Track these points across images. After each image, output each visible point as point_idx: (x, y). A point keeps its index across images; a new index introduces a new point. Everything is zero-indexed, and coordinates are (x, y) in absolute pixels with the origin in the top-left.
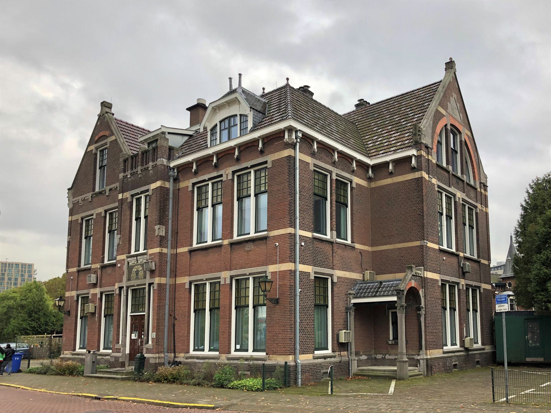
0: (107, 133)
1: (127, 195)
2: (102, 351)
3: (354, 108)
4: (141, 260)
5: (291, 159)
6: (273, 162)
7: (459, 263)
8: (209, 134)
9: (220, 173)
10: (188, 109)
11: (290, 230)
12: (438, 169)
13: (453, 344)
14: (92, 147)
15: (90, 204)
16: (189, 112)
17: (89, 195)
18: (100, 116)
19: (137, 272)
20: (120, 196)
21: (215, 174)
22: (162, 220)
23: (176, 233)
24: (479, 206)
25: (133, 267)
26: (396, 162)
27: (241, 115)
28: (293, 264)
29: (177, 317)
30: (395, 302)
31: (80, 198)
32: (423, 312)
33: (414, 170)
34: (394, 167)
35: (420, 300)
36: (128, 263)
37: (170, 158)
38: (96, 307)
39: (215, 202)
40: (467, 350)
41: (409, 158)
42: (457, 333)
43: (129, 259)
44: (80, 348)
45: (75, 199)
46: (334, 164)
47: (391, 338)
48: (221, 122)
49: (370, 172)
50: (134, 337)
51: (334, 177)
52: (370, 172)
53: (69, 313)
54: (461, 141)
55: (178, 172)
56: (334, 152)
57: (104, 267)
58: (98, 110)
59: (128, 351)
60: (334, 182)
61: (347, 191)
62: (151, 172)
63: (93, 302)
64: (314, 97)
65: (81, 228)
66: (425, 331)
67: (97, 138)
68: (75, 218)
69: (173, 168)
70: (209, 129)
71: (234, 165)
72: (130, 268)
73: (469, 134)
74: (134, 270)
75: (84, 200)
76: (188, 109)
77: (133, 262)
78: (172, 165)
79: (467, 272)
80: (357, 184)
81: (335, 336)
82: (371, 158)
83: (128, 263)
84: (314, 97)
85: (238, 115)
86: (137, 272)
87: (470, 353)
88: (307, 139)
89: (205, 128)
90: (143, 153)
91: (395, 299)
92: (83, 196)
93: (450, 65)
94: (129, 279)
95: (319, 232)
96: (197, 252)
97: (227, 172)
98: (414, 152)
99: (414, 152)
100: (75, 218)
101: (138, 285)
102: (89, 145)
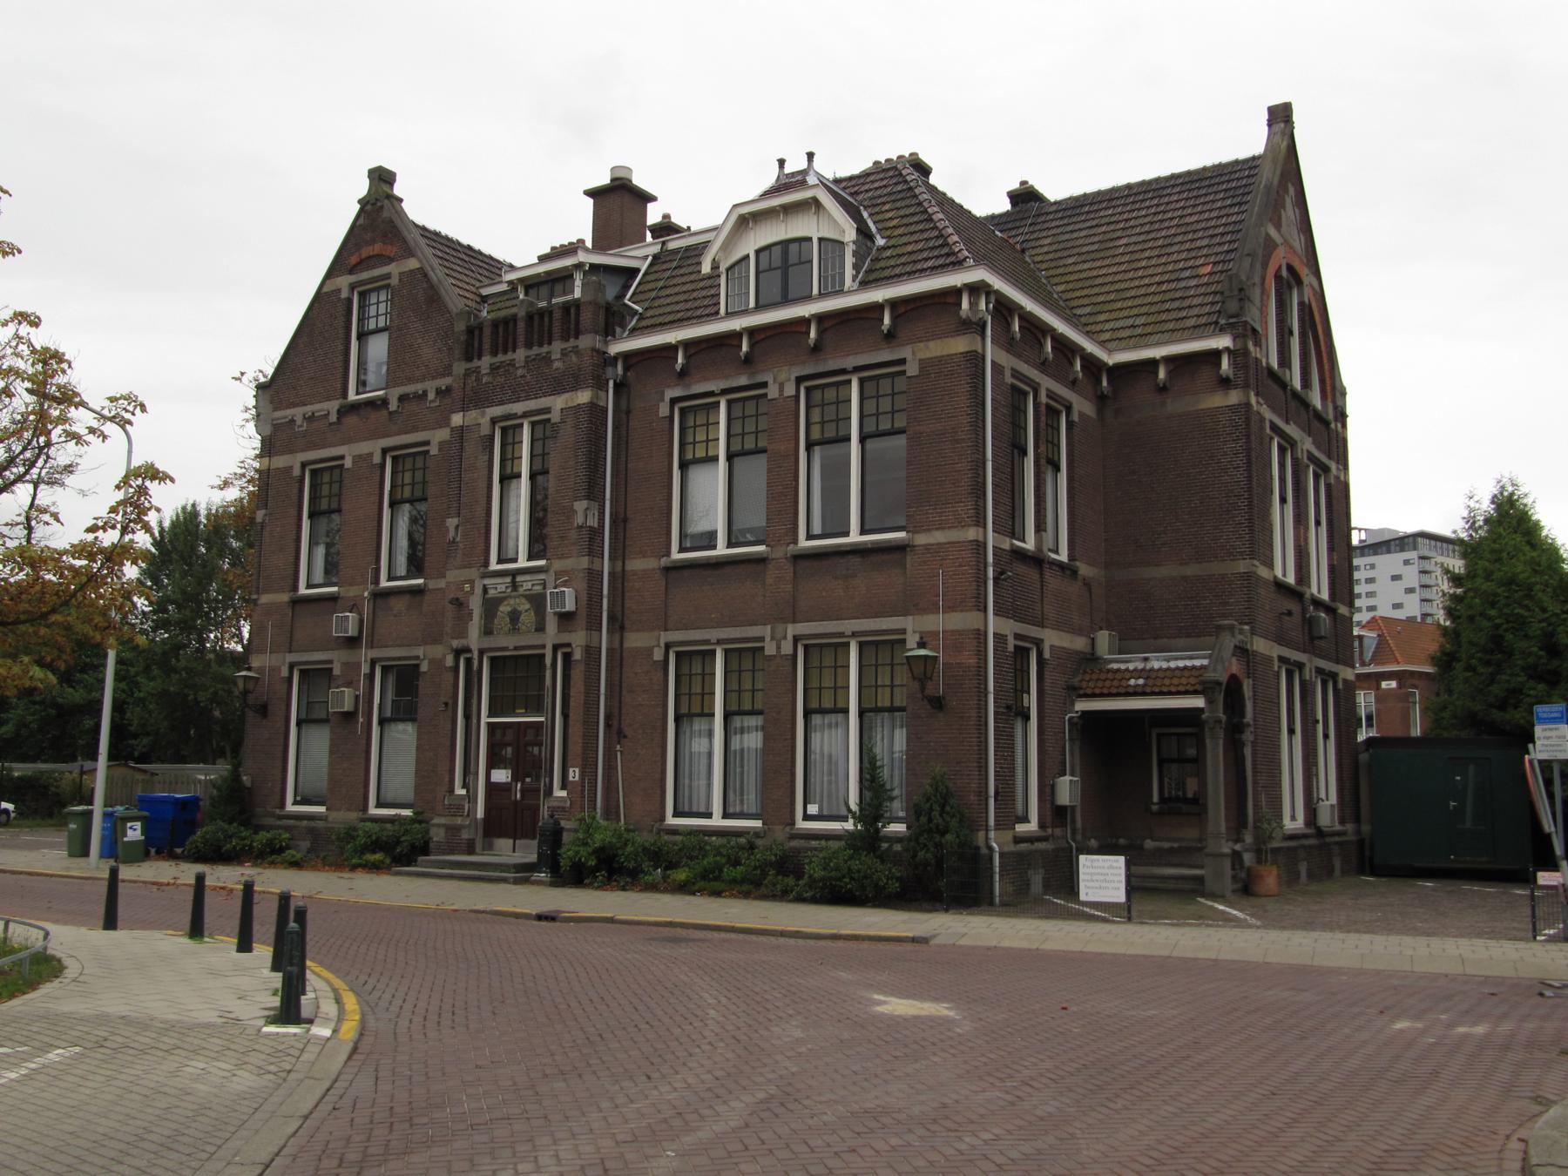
0: (390, 250)
1: (481, 418)
2: (290, 807)
3: (1004, 206)
4: (527, 586)
5: (976, 359)
6: (924, 365)
7: (1304, 611)
8: (723, 278)
9: (760, 379)
10: (590, 193)
11: (972, 534)
12: (1270, 382)
13: (1293, 818)
14: (344, 282)
15: (318, 431)
16: (591, 201)
17: (333, 406)
18: (363, 202)
19: (514, 616)
20: (457, 419)
21: (743, 381)
22: (593, 491)
23: (620, 521)
24: (1333, 466)
25: (498, 601)
26: (1178, 363)
27: (820, 240)
28: (981, 615)
29: (627, 731)
30: (1201, 710)
31: (298, 413)
32: (1248, 736)
33: (1225, 383)
34: (1169, 373)
35: (1243, 706)
36: (485, 590)
37: (608, 332)
38: (357, 697)
39: (736, 447)
40: (1320, 833)
41: (1215, 355)
42: (1304, 789)
43: (487, 581)
44: (295, 803)
45: (278, 414)
46: (1043, 366)
47: (1156, 799)
48: (758, 252)
49: (1105, 383)
50: (501, 776)
51: (1043, 399)
52: (1105, 383)
53: (263, 710)
54: (1301, 304)
55: (626, 369)
56: (1044, 336)
57: (381, 596)
58: (362, 187)
59: (480, 814)
60: (1043, 409)
61: (1058, 430)
62: (557, 365)
63: (349, 684)
64: (933, 180)
65: (301, 491)
66: (1255, 783)
67: (354, 260)
68: (280, 462)
69: (615, 358)
70: (723, 268)
71: (804, 363)
72: (491, 606)
73: (1316, 284)
74: (504, 609)
75: (310, 419)
76: (590, 193)
77: (502, 588)
78: (616, 348)
79: (1321, 638)
80: (1081, 414)
81: (1048, 790)
82: (1110, 345)
83: (485, 590)
84: (933, 180)
85: (815, 241)
86: (514, 616)
87: (1328, 840)
88: (1004, 308)
89: (715, 266)
90: (530, 317)
91: (1199, 702)
92: (309, 409)
93: (1281, 116)
94: (487, 631)
95: (1013, 535)
96: (686, 573)
97: (781, 381)
98: (1223, 342)
99: (1223, 342)
100: (280, 462)
101: (516, 648)
102: (330, 274)
